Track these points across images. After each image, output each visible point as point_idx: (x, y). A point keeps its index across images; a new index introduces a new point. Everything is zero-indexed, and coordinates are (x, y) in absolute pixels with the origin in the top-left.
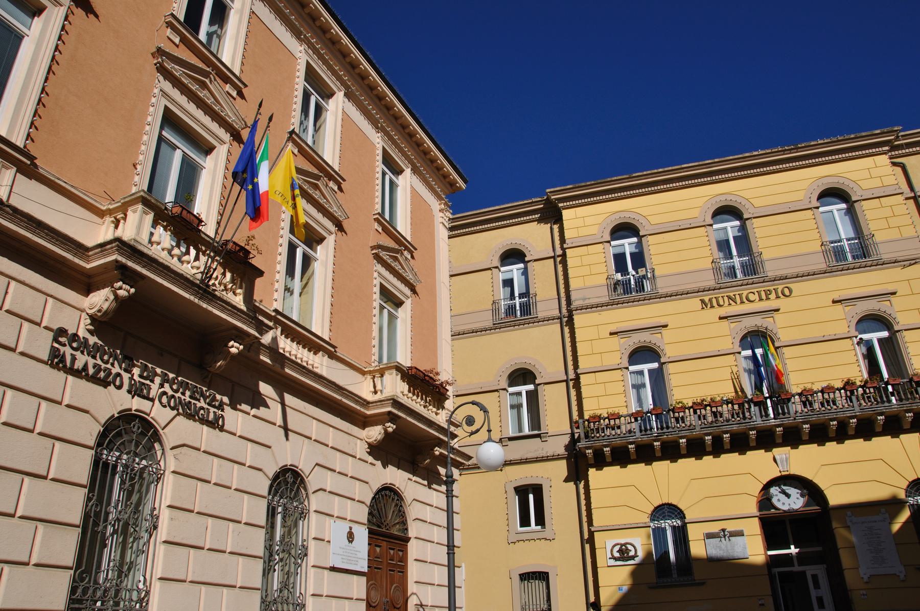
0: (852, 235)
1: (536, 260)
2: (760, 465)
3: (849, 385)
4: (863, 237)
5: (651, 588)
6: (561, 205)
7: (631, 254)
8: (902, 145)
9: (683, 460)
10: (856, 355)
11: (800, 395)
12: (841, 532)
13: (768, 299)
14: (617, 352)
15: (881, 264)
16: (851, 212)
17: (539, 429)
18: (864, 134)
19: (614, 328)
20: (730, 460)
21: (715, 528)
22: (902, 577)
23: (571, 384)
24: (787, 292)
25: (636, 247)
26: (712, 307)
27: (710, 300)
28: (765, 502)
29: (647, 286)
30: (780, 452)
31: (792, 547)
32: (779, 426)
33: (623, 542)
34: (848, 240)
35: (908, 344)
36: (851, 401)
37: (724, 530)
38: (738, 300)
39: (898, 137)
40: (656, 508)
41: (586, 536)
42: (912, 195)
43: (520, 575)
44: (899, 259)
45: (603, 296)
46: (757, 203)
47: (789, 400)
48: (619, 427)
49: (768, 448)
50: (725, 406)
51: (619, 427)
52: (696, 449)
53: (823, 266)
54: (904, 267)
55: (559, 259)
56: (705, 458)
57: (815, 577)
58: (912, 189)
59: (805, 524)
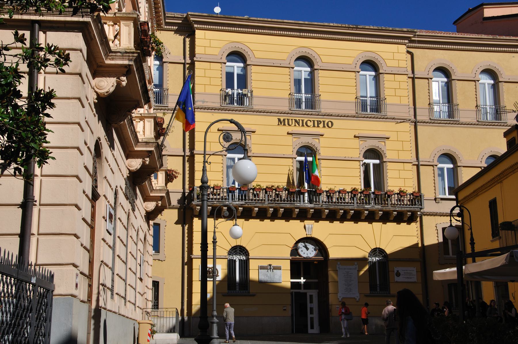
0: (374, 95)
1: (170, 63)
2: (297, 229)
3: (354, 192)
4: (380, 99)
5: (223, 296)
6: (196, 26)
7: (238, 75)
8: (416, 40)
9: (253, 220)
10: (360, 172)
11: (327, 192)
12: (331, 273)
13: (318, 126)
15: (385, 118)
16: (377, 79)
18: (397, 29)
20: (280, 224)
21: (265, 263)
22: (357, 299)
23: (187, 158)
24: (330, 125)
25: (242, 71)
26: (284, 125)
27: (284, 120)
28: (295, 251)
29: (246, 101)
30: (309, 223)
31: (302, 278)
32: (312, 208)
34: (371, 97)
35: (388, 171)
36: (353, 200)
37: (270, 265)
38: (301, 124)
39: (415, 35)
40: (232, 247)
41: (186, 260)
42: (412, 76)
43: (158, 282)
44: (396, 117)
45: (216, 102)
46: (324, 59)
47: (320, 194)
48: (219, 195)
49: (302, 220)
50: (284, 192)
51: (219, 195)
52: (262, 215)
53: (353, 113)
54: (397, 123)
55: (187, 66)
56: (265, 220)
58: (413, 72)
59: (314, 268)
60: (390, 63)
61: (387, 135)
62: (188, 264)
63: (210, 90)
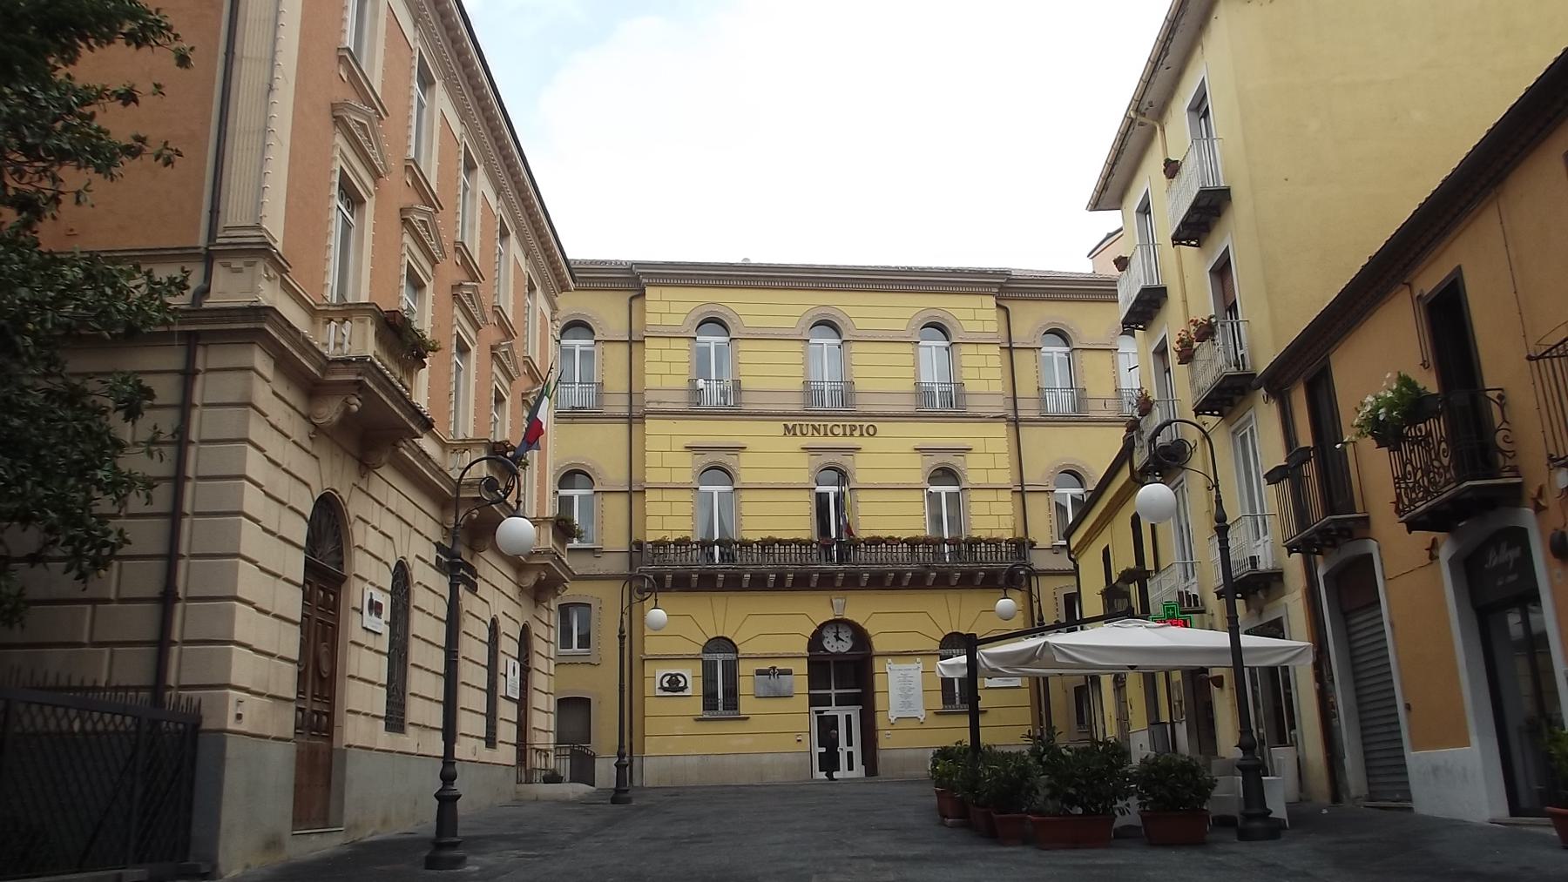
2: (815, 610)
14: (684, 469)
17: (1491, 470)
19: (689, 441)
21: (766, 665)
28: (816, 641)
33: (673, 672)
53: (911, 409)
57: (848, 718)
60: (968, 326)
61: (967, 444)
62: (1248, 474)
63: (669, 382)
